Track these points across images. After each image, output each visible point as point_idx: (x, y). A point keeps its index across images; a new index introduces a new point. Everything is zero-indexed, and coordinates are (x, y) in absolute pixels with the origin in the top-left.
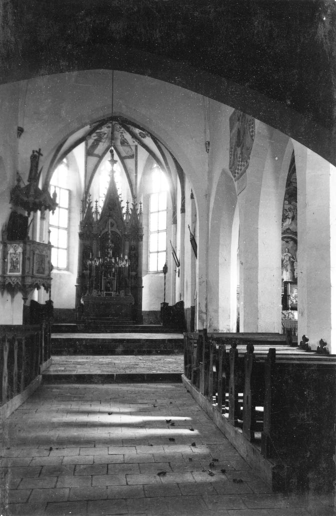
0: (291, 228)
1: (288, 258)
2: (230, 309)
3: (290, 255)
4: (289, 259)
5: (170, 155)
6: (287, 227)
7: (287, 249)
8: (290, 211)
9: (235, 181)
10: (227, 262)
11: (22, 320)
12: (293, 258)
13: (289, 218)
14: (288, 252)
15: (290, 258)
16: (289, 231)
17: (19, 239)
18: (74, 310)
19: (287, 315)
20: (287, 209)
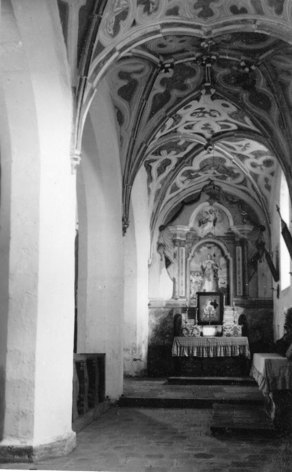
0: (213, 232)
1: (211, 266)
2: (136, 326)
3: (212, 262)
4: (212, 267)
5: (136, 144)
6: (208, 232)
7: (209, 256)
8: (211, 213)
9: (183, 174)
10: (278, 247)
11: (106, 384)
12: (217, 265)
13: (210, 221)
14: (211, 259)
15: (212, 265)
16: (211, 236)
17: (171, 89)
18: (254, 353)
19: (191, 331)
20: (208, 211)
